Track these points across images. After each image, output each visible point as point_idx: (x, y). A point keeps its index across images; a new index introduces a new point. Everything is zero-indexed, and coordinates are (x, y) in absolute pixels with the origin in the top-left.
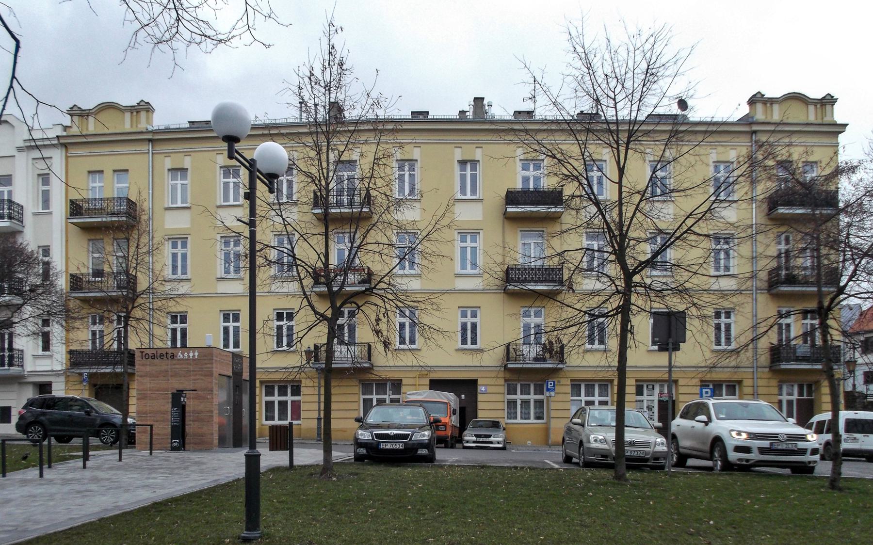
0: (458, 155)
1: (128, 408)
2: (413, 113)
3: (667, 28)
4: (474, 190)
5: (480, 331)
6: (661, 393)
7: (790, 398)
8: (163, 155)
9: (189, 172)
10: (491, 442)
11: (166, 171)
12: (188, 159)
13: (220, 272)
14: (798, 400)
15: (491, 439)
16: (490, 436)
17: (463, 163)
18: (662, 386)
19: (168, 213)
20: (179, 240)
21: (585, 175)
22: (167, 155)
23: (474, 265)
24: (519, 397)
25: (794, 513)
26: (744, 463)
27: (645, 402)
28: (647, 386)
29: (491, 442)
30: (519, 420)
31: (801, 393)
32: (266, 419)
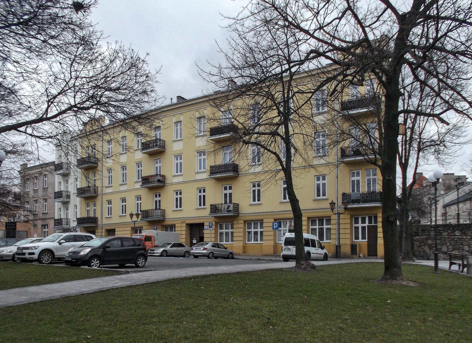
0: (175, 120)
1: (383, 230)
2: (179, 98)
3: (230, 39)
4: (181, 137)
5: (174, 204)
6: (290, 226)
7: (364, 225)
8: (172, 116)
9: (182, 122)
10: (154, 253)
11: (174, 124)
12: (182, 116)
13: (197, 169)
14: (368, 226)
15: (155, 251)
16: (154, 250)
17: (176, 123)
18: (291, 222)
19: (175, 143)
20: (178, 156)
21: (309, 95)
22: (174, 116)
23: (204, 168)
24: (224, 231)
25: (312, 289)
26: (31, 259)
27: (282, 230)
28: (283, 222)
29: (154, 253)
30: (253, 242)
31: (370, 222)
32: (355, 239)
